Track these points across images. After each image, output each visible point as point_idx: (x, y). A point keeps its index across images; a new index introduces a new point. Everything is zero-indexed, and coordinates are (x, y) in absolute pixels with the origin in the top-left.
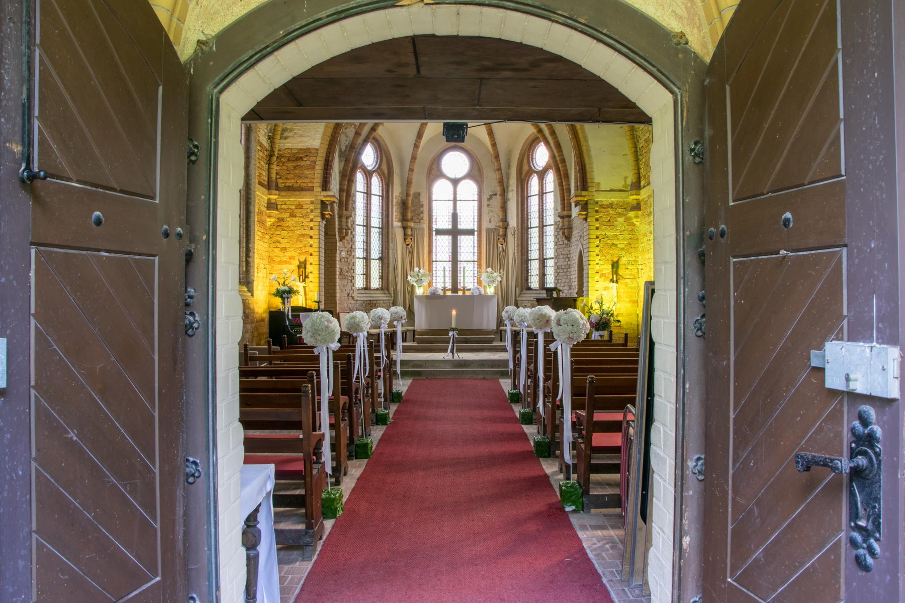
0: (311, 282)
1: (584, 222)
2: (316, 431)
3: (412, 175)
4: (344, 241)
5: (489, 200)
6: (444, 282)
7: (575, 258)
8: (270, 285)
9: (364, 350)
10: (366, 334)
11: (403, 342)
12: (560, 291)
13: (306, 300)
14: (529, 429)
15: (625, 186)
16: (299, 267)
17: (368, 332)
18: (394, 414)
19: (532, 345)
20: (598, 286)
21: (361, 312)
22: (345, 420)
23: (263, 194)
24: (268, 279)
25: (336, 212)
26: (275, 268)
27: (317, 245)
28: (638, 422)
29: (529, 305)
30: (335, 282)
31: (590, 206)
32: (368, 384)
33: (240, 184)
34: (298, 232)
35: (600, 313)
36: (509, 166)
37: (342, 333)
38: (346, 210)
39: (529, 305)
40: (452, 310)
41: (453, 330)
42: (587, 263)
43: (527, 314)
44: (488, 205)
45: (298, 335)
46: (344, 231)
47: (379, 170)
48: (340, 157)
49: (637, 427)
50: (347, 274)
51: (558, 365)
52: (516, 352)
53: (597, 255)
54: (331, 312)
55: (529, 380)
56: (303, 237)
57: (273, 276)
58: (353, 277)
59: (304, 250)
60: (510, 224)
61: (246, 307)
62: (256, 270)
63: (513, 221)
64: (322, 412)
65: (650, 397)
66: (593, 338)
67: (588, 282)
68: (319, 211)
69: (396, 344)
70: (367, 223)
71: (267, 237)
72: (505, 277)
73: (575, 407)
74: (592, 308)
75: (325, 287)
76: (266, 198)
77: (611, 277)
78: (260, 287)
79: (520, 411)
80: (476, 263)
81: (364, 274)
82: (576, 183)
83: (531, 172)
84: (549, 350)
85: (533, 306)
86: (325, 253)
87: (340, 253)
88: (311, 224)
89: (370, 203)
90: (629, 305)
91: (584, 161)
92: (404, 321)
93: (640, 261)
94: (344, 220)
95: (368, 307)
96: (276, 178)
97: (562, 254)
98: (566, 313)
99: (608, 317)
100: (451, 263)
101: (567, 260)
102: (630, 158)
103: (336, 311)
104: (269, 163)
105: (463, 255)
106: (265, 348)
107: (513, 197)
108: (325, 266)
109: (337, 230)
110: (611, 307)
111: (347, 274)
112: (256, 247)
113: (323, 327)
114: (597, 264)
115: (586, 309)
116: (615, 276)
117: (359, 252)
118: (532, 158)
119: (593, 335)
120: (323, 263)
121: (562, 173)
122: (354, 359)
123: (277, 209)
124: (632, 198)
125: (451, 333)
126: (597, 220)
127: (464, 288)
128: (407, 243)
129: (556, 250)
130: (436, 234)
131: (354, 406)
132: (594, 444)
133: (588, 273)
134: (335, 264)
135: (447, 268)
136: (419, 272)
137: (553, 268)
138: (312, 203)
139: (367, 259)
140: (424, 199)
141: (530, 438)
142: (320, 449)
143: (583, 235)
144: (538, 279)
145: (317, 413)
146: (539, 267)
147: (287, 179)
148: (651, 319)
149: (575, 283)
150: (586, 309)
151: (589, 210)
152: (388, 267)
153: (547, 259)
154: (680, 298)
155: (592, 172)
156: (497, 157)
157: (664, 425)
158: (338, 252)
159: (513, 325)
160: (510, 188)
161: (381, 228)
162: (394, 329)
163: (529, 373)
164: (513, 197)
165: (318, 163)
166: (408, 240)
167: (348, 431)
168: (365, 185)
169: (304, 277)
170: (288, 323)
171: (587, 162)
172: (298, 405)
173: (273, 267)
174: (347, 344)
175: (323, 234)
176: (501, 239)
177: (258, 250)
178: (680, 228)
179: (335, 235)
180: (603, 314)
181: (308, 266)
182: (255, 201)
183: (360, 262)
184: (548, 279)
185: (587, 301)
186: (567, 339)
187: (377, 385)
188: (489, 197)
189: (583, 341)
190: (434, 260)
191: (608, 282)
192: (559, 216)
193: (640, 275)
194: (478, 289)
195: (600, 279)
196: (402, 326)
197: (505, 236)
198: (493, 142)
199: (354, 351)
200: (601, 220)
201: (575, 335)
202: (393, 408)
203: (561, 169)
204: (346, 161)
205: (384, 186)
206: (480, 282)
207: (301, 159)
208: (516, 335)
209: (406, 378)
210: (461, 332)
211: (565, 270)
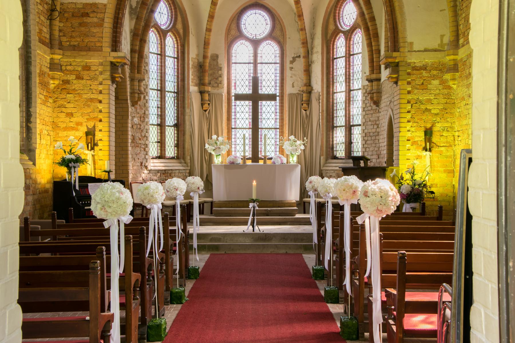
0: (101, 150)
1: (395, 85)
2: (104, 312)
3: (209, 35)
4: (136, 106)
5: (292, 62)
6: (244, 151)
7: (384, 124)
8: (54, 153)
9: (158, 223)
11: (200, 214)
12: (368, 160)
13: (95, 169)
14: (336, 309)
15: (442, 45)
16: (87, 134)
17: (162, 204)
18: (190, 292)
20: (409, 154)
21: (156, 182)
22: (137, 299)
23: (45, 53)
24: (52, 146)
25: (128, 75)
26: (60, 135)
27: (107, 110)
28: (455, 302)
29: (334, 175)
30: (127, 150)
31: (401, 68)
32: (162, 259)
33: (19, 42)
34: (85, 96)
35: (411, 183)
36: (314, 25)
37: (135, 205)
38: (138, 73)
39: (334, 175)
41: (253, 201)
42: (397, 130)
43: (332, 185)
44: (291, 68)
45: (86, 208)
47: (173, 29)
48: (131, 14)
49: (455, 308)
50: (140, 142)
52: (321, 225)
53: (409, 121)
54: (122, 182)
55: (335, 256)
56: (91, 102)
57: (58, 143)
58: (146, 146)
59: (92, 115)
60: (314, 88)
61: (28, 176)
62: (38, 137)
63: (317, 85)
64: (112, 291)
65: (469, 276)
66: (404, 211)
67: (398, 150)
69: (192, 216)
70: (161, 87)
71: (51, 100)
72: (308, 146)
73: (384, 286)
76: (49, 58)
77: (424, 145)
78: (43, 156)
79: (325, 289)
80: (278, 130)
81: (158, 142)
82: (386, 43)
83: (337, 32)
84: (356, 223)
85: (338, 176)
86: (116, 119)
87: (132, 120)
88: (101, 88)
89: (165, 65)
90: (444, 176)
91: (396, 18)
92: (201, 192)
93: (456, 127)
94: (136, 83)
95: (163, 177)
96: (60, 36)
97: (370, 121)
98: (374, 184)
99: (420, 189)
100: (251, 130)
101: (375, 127)
102: (448, 14)
103: (128, 181)
104: (51, 19)
105: (264, 122)
106: (49, 222)
107: (317, 59)
108: (116, 133)
109: (129, 94)
110: (423, 178)
111: (140, 142)
112: (38, 112)
113: (114, 199)
114: (409, 131)
115: (397, 179)
116: (428, 144)
117: (153, 118)
118: (339, 16)
119: (404, 208)
120: (113, 130)
121: (371, 32)
123: (61, 70)
124: (448, 59)
125: (251, 205)
126: (409, 83)
127: (265, 157)
128: (204, 109)
129: (364, 117)
130: (236, 99)
131: (147, 283)
132: (406, 327)
133: (398, 141)
135: (247, 135)
136: (217, 139)
137: (360, 136)
138: (101, 64)
139: (162, 126)
140: (222, 62)
141: (336, 318)
142: (109, 331)
143: (393, 100)
144: (344, 147)
145: (106, 292)
146: (346, 135)
147: (71, 37)
148: (468, 190)
149: (384, 152)
150: (397, 179)
151: (401, 73)
152: (184, 135)
153: (354, 126)
154: (501, 168)
155: (405, 30)
156: (300, 16)
157: (486, 307)
158: (130, 118)
160: (315, 50)
161: (176, 93)
162: (191, 200)
164: (317, 59)
165: (106, 20)
166: (206, 106)
167: (140, 311)
168: (159, 46)
169: (92, 145)
170: (74, 194)
171: (399, 19)
172: (85, 284)
173: (58, 134)
174: (140, 217)
175: (114, 98)
176: (305, 105)
177: (40, 115)
178: (502, 90)
179: (127, 100)
180: (415, 185)
181: (97, 133)
182: (36, 61)
183: (154, 129)
184: (355, 147)
185: (398, 171)
186: (375, 212)
187: (172, 260)
188: (292, 59)
189: (392, 214)
190: (233, 127)
191: (420, 150)
192: (367, 80)
193: (456, 142)
195: (411, 148)
196: (199, 197)
197: (309, 102)
198: (299, 6)
199: (147, 225)
200: (413, 84)
201: (384, 207)
202: (189, 285)
203: (370, 28)
204: (137, 19)
205: (179, 47)
207: (87, 15)
208: (321, 207)
210: (262, 203)
211: (373, 138)
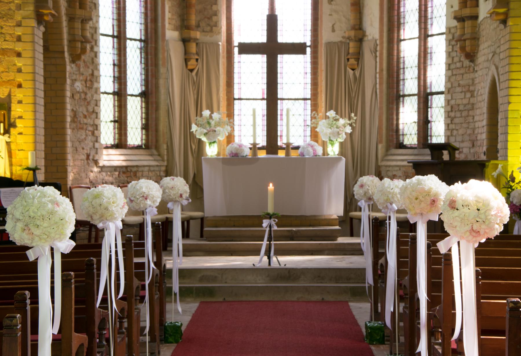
0: (21, 134)
1: (502, 26)
4: (78, 62)
6: (254, 136)
10: (120, 225)
11: (183, 237)
13: (11, 165)
17: (122, 221)
19: (405, 243)
21: (112, 187)
25: (63, 11)
27: (30, 69)
29: (399, 173)
30: (64, 134)
32: (122, 310)
37: (79, 224)
38: (81, 8)
40: (269, 183)
41: (269, 216)
43: (397, 191)
46: (79, 45)
50: (85, 121)
51: (452, 278)
54: (57, 187)
55: (402, 305)
58: (96, 127)
60: (368, 33)
66: (515, 233)
68: (31, 8)
69: (171, 241)
72: (358, 126)
74: (513, 179)
75: (45, 143)
84: (437, 252)
85: (407, 176)
86: (45, 83)
87: (72, 85)
88: (19, 31)
92: (185, 203)
94: (78, 25)
95: (123, 178)
97: (459, 85)
100: (265, 102)
101: (468, 95)
103: (66, 184)
109: (66, 42)
111: (85, 121)
113: (44, 213)
115: (503, 181)
119: (516, 228)
120: (42, 102)
122: (99, 269)
125: (265, 223)
127: (288, 145)
128: (190, 67)
129: (449, 79)
131: (98, 350)
134: (64, 103)
136: (211, 117)
137: (443, 110)
143: (498, 51)
149: (483, 136)
150: (503, 181)
152: (157, 109)
153: (432, 94)
158: (68, 81)
159: (373, 208)
161: (144, 41)
162: (168, 216)
163: (401, 292)
166: (192, 63)
174: (86, 242)
176: (352, 61)
179: (63, 52)
183: (136, 102)
185: (505, 168)
186: (468, 233)
187: (139, 313)
189: (497, 237)
192: (455, 18)
194: (312, 146)
196: (182, 210)
197: (359, 56)
199: (98, 255)
201: (483, 227)
206: (315, 135)
209: (189, 300)
211: (464, 114)
